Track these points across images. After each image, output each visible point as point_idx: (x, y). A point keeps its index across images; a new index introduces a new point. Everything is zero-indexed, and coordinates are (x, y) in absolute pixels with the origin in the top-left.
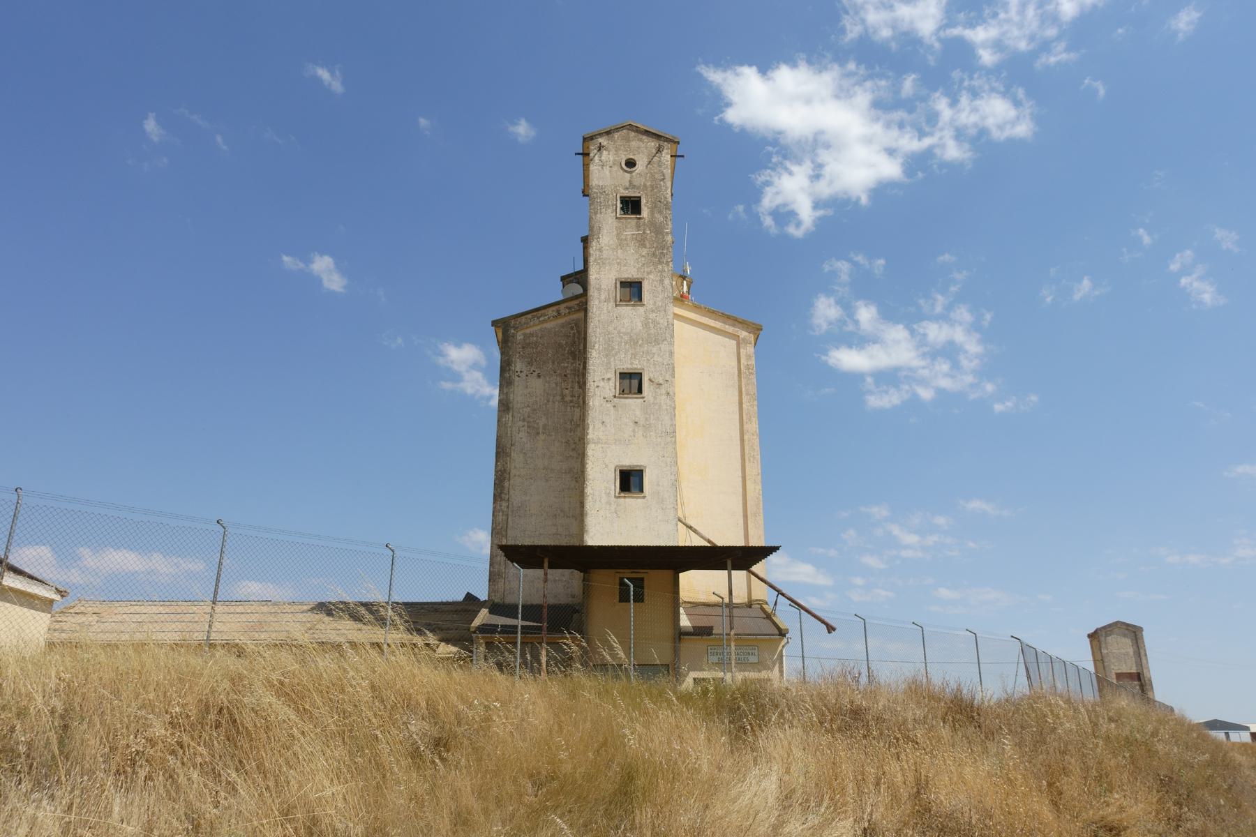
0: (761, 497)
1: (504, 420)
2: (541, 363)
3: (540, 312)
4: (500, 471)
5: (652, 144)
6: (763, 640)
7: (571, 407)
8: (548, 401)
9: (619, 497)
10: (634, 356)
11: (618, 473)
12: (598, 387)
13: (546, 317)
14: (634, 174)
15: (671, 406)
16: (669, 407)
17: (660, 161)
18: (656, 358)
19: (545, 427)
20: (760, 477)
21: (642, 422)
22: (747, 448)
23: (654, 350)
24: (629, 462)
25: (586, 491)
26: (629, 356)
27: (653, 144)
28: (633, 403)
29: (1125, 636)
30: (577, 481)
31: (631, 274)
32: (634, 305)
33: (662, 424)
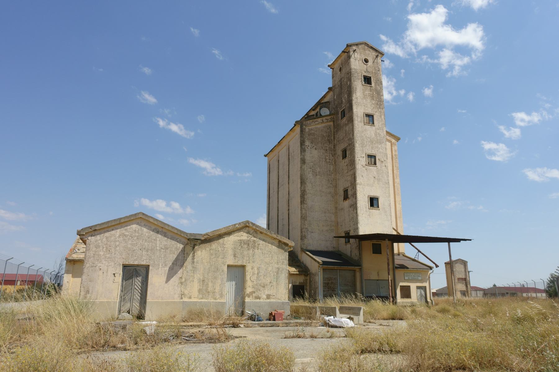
0: (402, 210)
1: (303, 167)
2: (316, 143)
3: (315, 120)
4: (303, 190)
5: (374, 54)
6: (423, 271)
7: (329, 164)
8: (320, 161)
9: (370, 209)
10: (372, 148)
11: (369, 198)
12: (359, 160)
13: (318, 122)
14: (368, 66)
15: (387, 171)
16: (386, 172)
17: (377, 62)
18: (380, 150)
19: (319, 172)
20: (401, 202)
21: (376, 178)
22: (396, 189)
23: (380, 146)
24: (373, 194)
25: (357, 205)
26: (370, 148)
27: (374, 53)
28: (373, 168)
29: (461, 264)
30: (333, 198)
31: (370, 111)
32: (371, 125)
33: (384, 179)
